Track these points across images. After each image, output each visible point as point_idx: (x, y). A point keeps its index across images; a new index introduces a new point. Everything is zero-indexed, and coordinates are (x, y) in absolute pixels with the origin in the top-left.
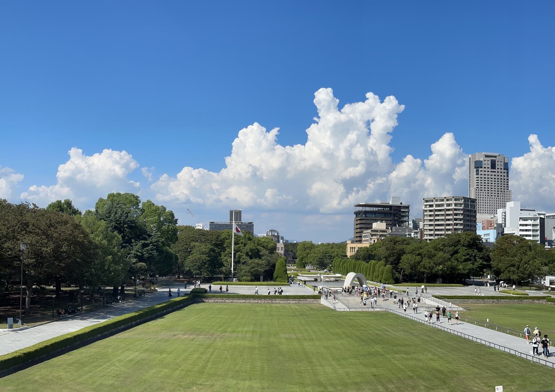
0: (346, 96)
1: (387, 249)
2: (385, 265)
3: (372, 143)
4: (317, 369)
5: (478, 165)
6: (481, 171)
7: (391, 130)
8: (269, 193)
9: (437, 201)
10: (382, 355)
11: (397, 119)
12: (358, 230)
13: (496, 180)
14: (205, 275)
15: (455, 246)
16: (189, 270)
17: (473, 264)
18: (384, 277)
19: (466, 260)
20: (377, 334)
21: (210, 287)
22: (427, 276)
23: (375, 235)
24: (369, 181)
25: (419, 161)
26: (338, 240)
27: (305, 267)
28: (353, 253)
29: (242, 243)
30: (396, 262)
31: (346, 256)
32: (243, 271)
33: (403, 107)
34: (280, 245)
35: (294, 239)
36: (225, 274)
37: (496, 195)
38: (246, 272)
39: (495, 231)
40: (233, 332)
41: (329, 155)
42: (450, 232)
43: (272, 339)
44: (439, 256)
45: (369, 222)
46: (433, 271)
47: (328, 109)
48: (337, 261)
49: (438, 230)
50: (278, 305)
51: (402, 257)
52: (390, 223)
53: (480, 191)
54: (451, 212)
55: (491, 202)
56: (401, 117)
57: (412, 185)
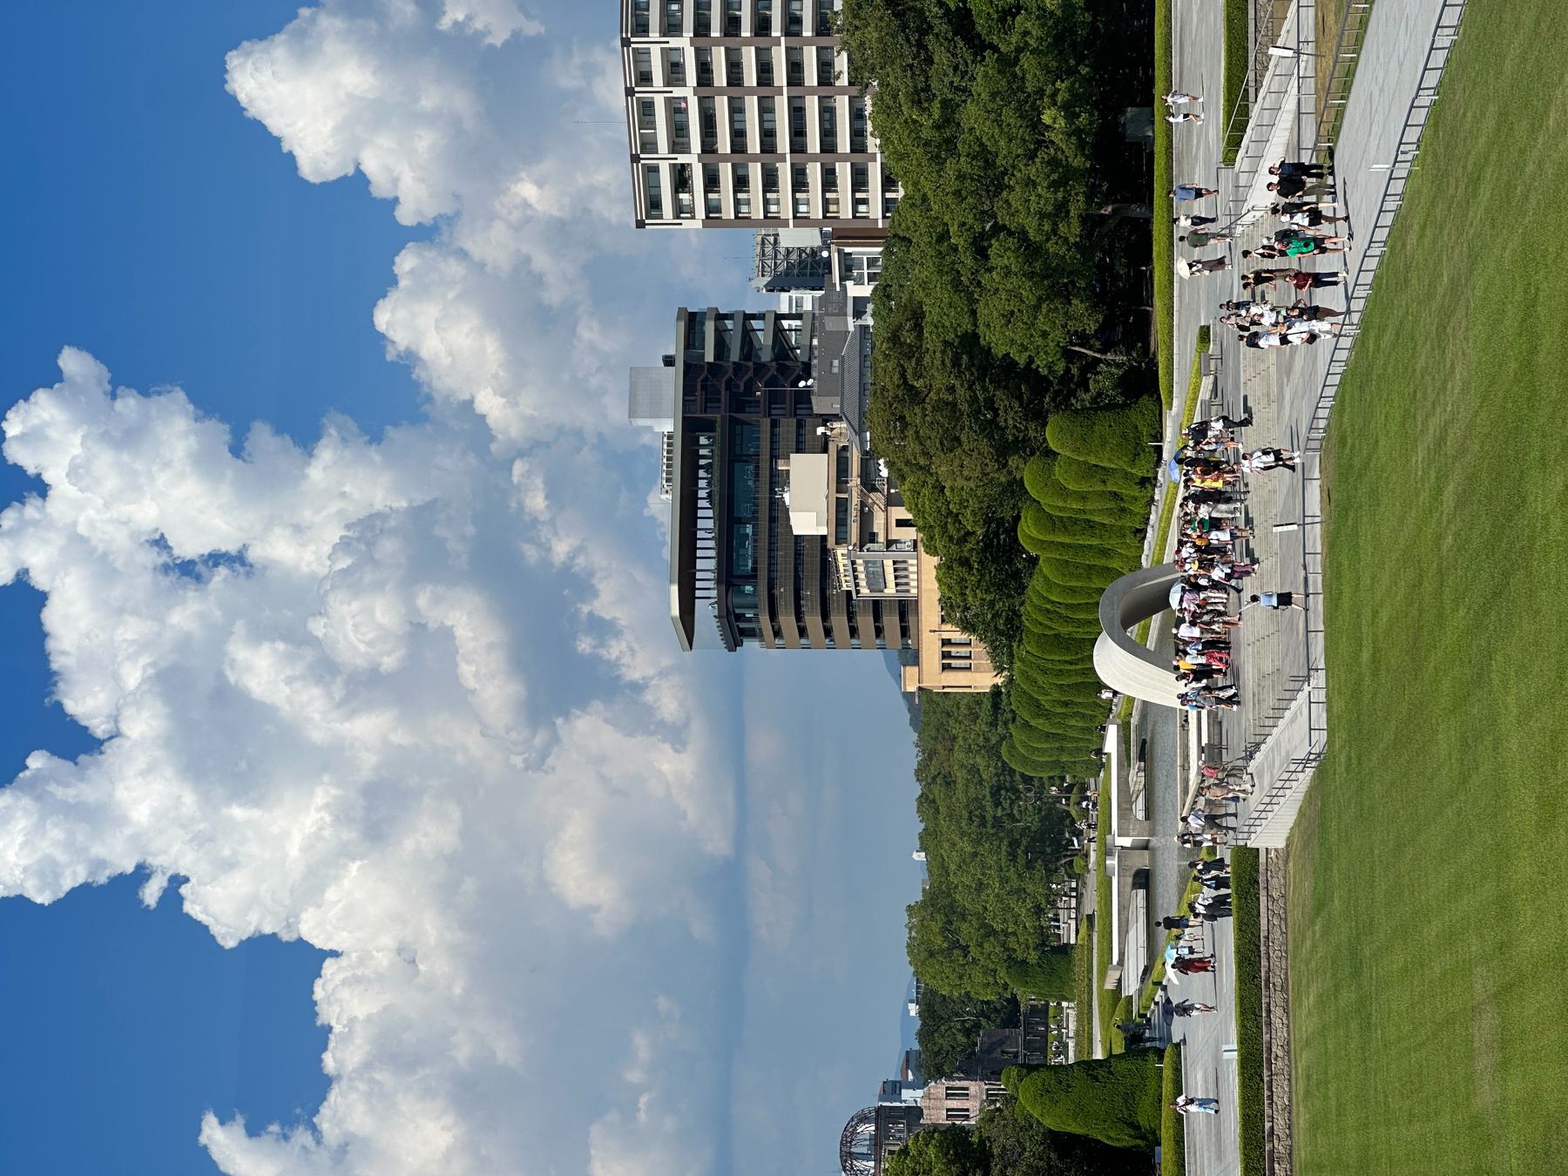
1: (952, 442)
2: (1050, 454)
3: (298, 548)
7: (220, 432)
9: (649, 145)
11: (145, 392)
12: (839, 622)
15: (925, 28)
18: (1122, 464)
20: (1462, 501)
23: (866, 518)
24: (531, 553)
25: (406, 262)
26: (901, 750)
27: (1065, 950)
28: (979, 649)
30: (1038, 391)
31: (996, 692)
33: (71, 361)
34: (935, 1102)
35: (897, 1018)
41: (376, 813)
42: (841, 63)
44: (985, 130)
45: (785, 557)
46: (1078, 162)
47: (96, 816)
48: (1027, 751)
49: (828, 134)
50: (1302, 1121)
51: (999, 351)
52: (788, 427)
54: (719, 58)
56: (134, 371)
57: (554, 296)
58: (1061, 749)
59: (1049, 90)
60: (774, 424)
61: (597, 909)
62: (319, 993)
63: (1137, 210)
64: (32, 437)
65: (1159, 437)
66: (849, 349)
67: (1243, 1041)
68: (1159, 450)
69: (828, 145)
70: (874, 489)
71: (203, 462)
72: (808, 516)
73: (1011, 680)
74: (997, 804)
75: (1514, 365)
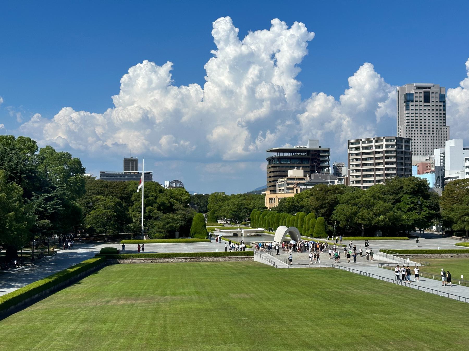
0: (247, 24)
1: (318, 199)
2: (316, 218)
4: (295, 330)
5: (408, 99)
6: (412, 105)
7: (299, 62)
8: (164, 140)
9: (364, 142)
10: (359, 315)
11: (307, 48)
12: (272, 179)
13: (431, 115)
14: (111, 232)
15: (397, 194)
16: (91, 228)
17: (419, 214)
18: (315, 231)
19: (410, 210)
21: (124, 246)
22: (365, 228)
25: (331, 97)
29: (152, 196)
30: (328, 215)
32: (156, 227)
36: (133, 231)
37: (431, 133)
38: (159, 228)
39: (434, 175)
40: (174, 294)
41: (228, 93)
43: (224, 300)
45: (284, 169)
46: (373, 222)
47: (227, 42)
48: (255, 214)
49: (366, 176)
52: (308, 169)
53: (411, 129)
55: (424, 141)
56: (311, 45)
58: (256, 220)
59: (387, 217)
60: (309, 167)
61: (212, 135)
62: (196, 84)
63: (363, 233)
64: (299, 27)
65: (320, 238)
66: (324, 180)
67: (219, 253)
68: (318, 238)
69: (364, 176)
70: (297, 185)
71: (294, 59)
72: (291, 173)
73: (269, 211)
74: (244, 208)
75: (370, 302)
